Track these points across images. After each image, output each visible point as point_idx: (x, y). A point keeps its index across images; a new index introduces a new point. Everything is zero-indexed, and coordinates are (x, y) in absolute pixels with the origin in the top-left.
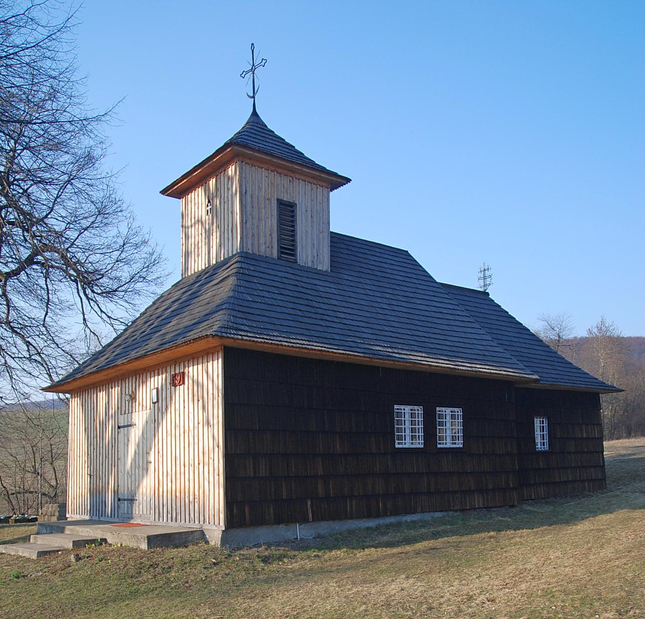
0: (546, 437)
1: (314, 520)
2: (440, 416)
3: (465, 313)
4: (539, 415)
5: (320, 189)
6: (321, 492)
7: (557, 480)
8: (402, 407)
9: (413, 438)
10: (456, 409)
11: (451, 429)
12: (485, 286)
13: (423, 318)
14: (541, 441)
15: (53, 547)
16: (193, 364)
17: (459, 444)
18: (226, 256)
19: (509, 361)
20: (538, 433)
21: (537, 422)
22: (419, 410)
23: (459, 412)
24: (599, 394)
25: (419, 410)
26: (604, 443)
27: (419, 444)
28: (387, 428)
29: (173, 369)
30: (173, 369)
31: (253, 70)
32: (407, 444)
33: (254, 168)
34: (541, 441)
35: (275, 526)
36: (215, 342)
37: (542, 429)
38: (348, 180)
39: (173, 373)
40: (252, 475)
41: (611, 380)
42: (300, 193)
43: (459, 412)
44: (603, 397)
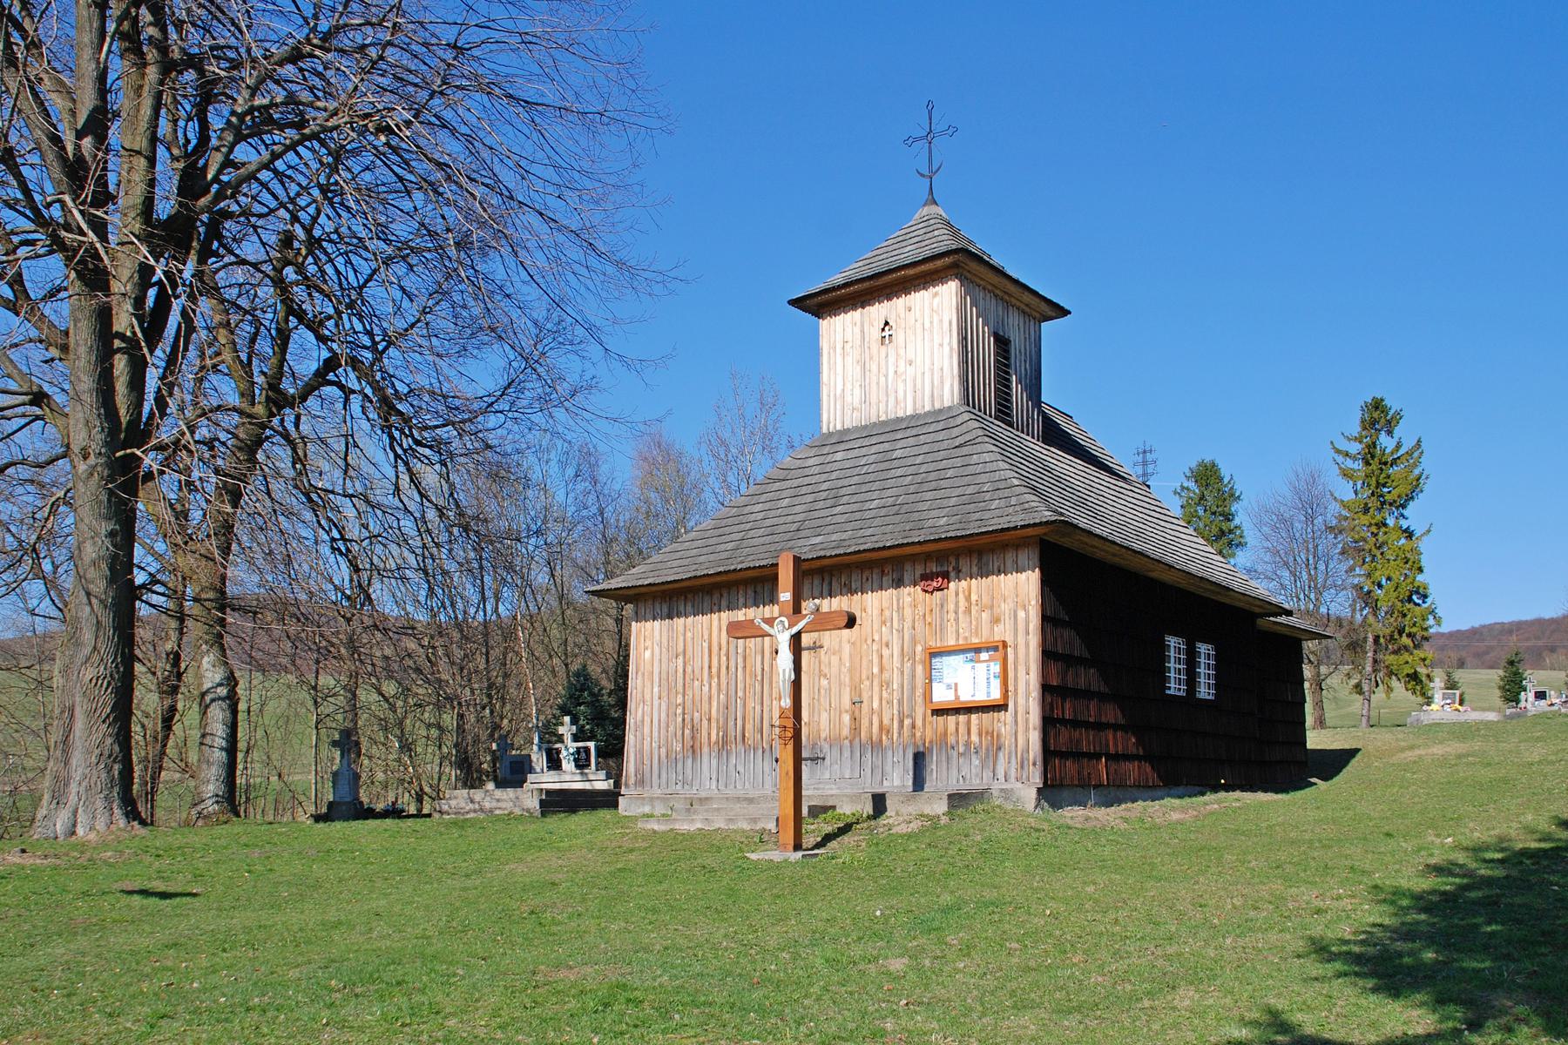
12: (1144, 475)
24: (1300, 641)
31: (929, 136)
38: (1064, 312)
44: (1309, 646)
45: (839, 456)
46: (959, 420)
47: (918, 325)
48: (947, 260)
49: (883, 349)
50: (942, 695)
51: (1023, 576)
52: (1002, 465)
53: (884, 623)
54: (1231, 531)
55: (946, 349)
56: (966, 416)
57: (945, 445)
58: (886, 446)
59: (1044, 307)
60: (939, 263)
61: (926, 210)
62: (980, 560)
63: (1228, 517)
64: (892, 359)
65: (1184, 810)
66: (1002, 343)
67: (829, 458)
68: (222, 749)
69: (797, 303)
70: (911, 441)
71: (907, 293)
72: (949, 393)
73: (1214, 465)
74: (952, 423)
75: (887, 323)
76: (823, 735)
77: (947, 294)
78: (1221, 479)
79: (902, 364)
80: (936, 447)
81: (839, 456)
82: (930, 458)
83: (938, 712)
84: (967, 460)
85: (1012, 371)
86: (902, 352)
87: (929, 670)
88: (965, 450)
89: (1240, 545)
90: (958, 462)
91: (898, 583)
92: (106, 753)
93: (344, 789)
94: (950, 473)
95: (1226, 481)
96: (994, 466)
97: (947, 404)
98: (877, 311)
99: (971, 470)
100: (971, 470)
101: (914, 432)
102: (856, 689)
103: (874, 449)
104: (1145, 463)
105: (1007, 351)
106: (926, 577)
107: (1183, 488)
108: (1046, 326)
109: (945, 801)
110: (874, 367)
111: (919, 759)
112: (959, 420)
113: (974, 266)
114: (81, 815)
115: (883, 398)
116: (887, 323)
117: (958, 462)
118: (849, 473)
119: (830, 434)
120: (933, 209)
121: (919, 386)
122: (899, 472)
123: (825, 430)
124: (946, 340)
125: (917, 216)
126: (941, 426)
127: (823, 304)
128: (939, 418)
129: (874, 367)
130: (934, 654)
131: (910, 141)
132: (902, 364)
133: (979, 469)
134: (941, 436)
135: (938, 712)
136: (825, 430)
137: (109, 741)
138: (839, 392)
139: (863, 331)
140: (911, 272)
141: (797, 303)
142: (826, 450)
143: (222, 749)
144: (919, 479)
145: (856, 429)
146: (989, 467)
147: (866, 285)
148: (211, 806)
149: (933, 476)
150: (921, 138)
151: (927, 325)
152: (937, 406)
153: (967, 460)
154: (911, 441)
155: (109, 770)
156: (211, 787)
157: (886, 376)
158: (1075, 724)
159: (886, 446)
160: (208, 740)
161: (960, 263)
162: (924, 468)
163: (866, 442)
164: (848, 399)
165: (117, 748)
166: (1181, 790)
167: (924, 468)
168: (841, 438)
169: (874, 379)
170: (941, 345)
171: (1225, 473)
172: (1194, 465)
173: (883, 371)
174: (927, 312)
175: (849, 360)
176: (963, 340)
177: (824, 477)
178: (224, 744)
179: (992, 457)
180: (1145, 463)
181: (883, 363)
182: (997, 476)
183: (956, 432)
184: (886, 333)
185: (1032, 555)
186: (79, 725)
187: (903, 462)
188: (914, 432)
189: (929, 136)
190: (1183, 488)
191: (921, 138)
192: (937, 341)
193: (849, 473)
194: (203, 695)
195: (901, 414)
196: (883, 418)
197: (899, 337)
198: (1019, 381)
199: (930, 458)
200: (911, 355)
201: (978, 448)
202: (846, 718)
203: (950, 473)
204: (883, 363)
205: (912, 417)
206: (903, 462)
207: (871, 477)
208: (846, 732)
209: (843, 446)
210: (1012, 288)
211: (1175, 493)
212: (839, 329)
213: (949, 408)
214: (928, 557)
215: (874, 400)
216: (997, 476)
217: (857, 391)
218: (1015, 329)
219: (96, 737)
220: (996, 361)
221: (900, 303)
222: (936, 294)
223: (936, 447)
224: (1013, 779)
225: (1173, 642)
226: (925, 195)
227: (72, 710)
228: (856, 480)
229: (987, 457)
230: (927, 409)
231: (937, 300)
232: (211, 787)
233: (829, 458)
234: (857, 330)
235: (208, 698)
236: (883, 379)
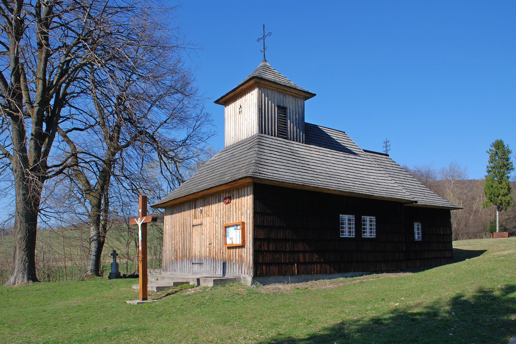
0: (420, 233)
1: (298, 273)
2: (364, 221)
3: (377, 166)
4: (417, 221)
5: (299, 100)
6: (302, 260)
7: (426, 257)
8: (344, 216)
9: (350, 232)
10: (372, 217)
11: (369, 231)
12: (386, 151)
13: (354, 168)
14: (417, 236)
15: (178, 279)
16: (195, 206)
17: (374, 235)
18: (252, 135)
19: (401, 191)
20: (416, 231)
21: (416, 225)
22: (352, 217)
23: (373, 218)
24: (449, 210)
25: (352, 217)
26: (453, 242)
27: (353, 235)
28: (337, 225)
29: (224, 195)
30: (224, 195)
31: (264, 37)
32: (346, 235)
33: (265, 89)
34: (417, 236)
35: (278, 276)
36: (250, 180)
37: (418, 229)
38: (315, 95)
39: (224, 197)
40: (266, 249)
41: (456, 204)
42: (290, 103)
43: (373, 218)
44: (452, 212)
50: (229, 242)
51: (249, 197)
53: (216, 215)
54: (508, 164)
62: (238, 192)
63: (507, 160)
65: (373, 278)
68: (94, 255)
69: (217, 102)
73: (501, 141)
76: (203, 255)
78: (504, 146)
83: (229, 248)
87: (226, 230)
89: (512, 169)
91: (219, 201)
92: (23, 260)
93: (114, 269)
95: (506, 146)
102: (210, 239)
104: (386, 146)
106: (225, 199)
107: (490, 150)
109: (212, 282)
111: (224, 264)
113: (263, 82)
114: (17, 278)
130: (226, 227)
131: (259, 40)
135: (229, 248)
137: (24, 256)
141: (217, 102)
143: (94, 255)
148: (89, 273)
150: (262, 38)
155: (24, 265)
156: (90, 267)
158: (276, 252)
160: (90, 253)
161: (257, 82)
165: (27, 258)
166: (351, 274)
171: (505, 144)
172: (494, 142)
176: (260, 110)
178: (95, 254)
180: (386, 146)
185: (250, 190)
186: (17, 252)
189: (264, 37)
190: (490, 150)
192: (253, 111)
194: (90, 239)
200: (246, 118)
202: (208, 249)
208: (208, 254)
211: (487, 152)
214: (226, 191)
218: (290, 103)
219: (21, 255)
221: (244, 98)
224: (246, 274)
225: (345, 218)
226: (263, 58)
227: (16, 247)
232: (90, 267)
235: (91, 240)
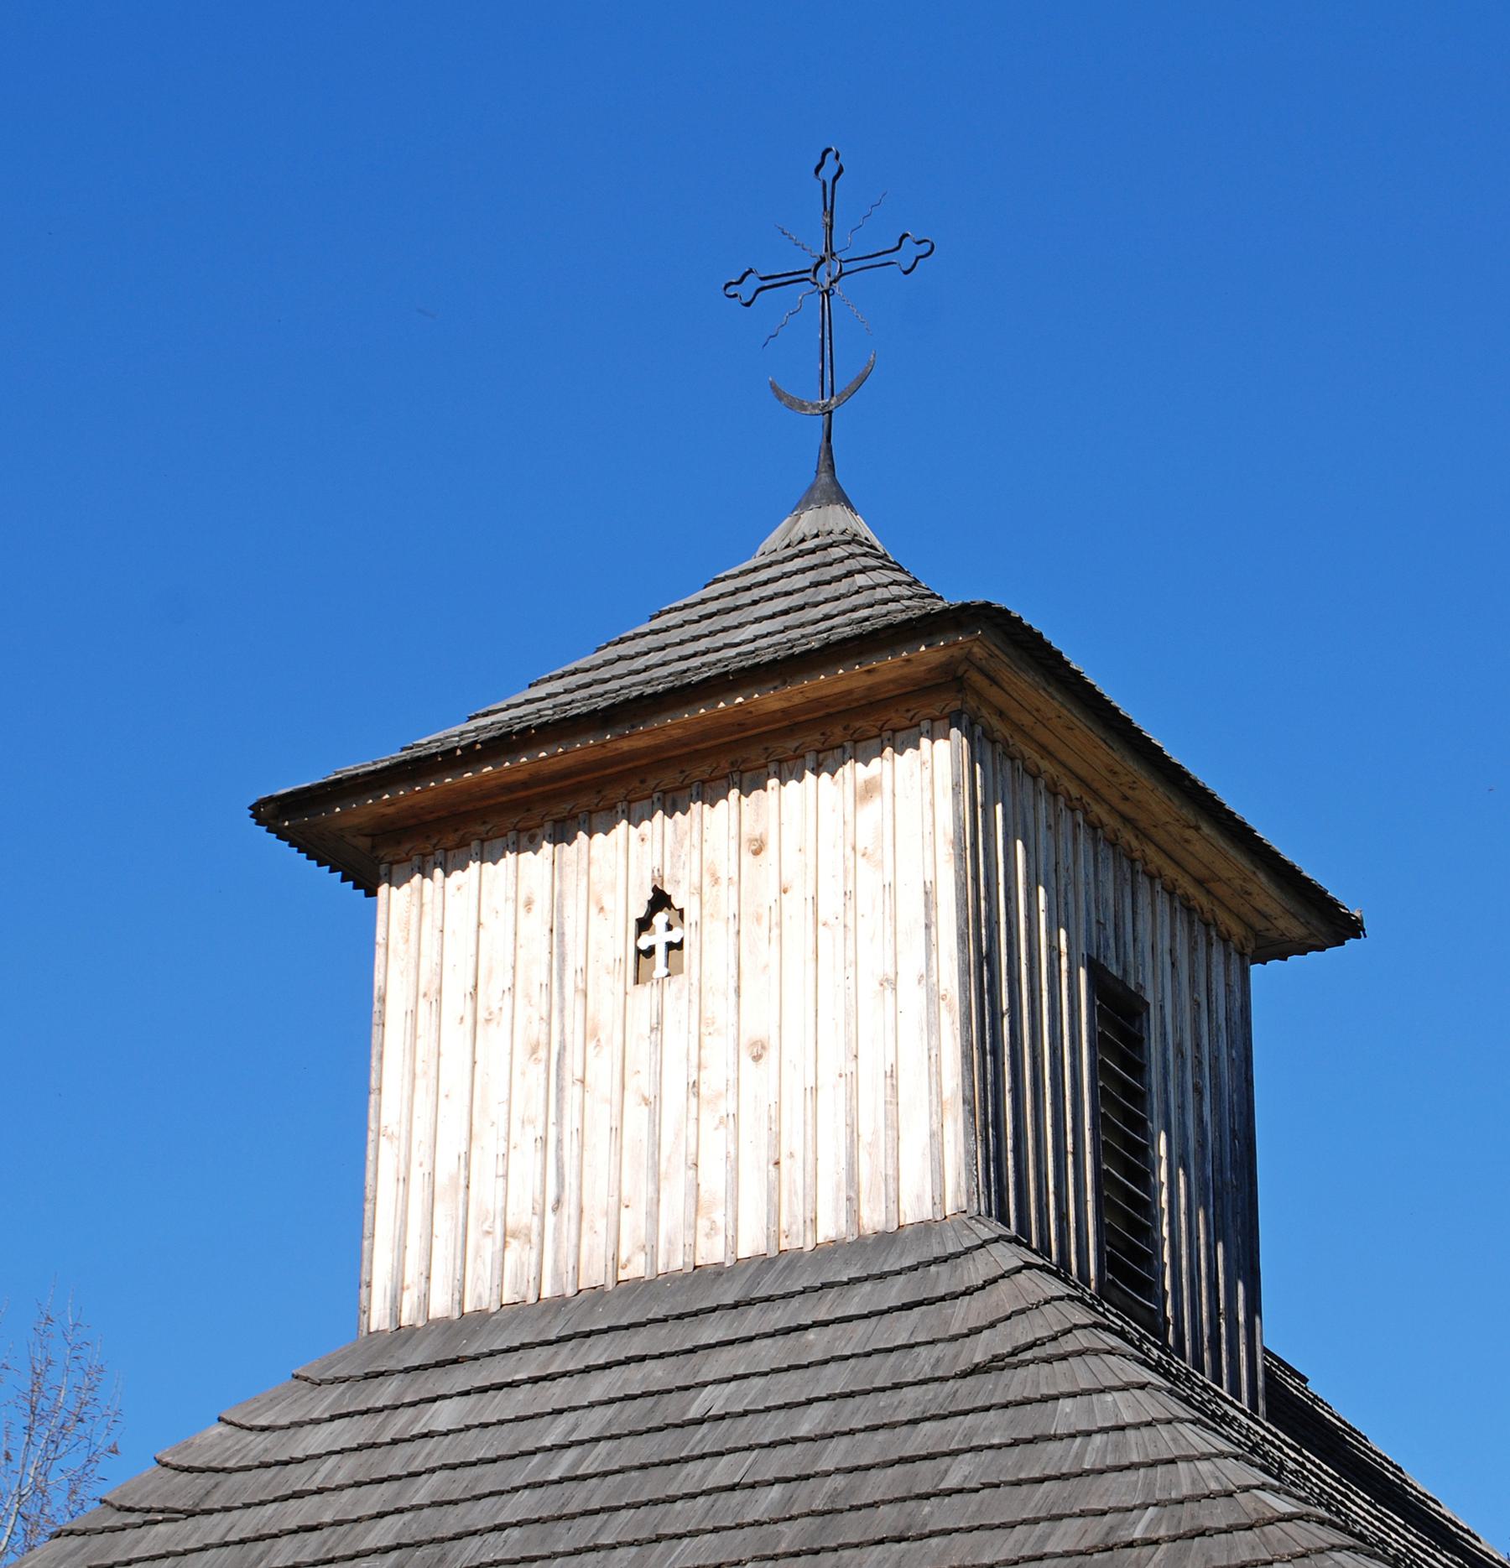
38: (1339, 926)
45: (444, 1415)
46: (976, 1270)
47: (795, 905)
48: (925, 654)
49: (644, 995)
52: (1197, 1439)
55: (913, 997)
56: (1007, 1256)
57: (923, 1362)
58: (657, 1374)
59: (1266, 895)
60: (889, 666)
61: (808, 522)
64: (677, 1038)
66: (1119, 1014)
67: (399, 1424)
70: (768, 1353)
71: (751, 782)
72: (921, 1165)
74: (943, 1280)
75: (660, 900)
77: (923, 783)
79: (719, 1052)
80: (883, 1371)
81: (444, 1415)
82: (858, 1413)
84: (1030, 1421)
85: (1155, 1125)
86: (719, 1007)
88: (1017, 1383)
90: (995, 1428)
94: (958, 1473)
96: (1163, 1442)
97: (915, 1209)
98: (617, 860)
99: (1051, 1458)
100: (1051, 1458)
101: (779, 1316)
103: (600, 1386)
105: (1137, 1042)
108: (1269, 980)
110: (602, 1070)
112: (976, 1270)
113: (1023, 687)
115: (637, 1187)
116: (660, 900)
117: (995, 1428)
118: (490, 1478)
119: (402, 1335)
120: (837, 518)
121: (793, 1141)
122: (722, 1471)
123: (378, 1318)
124: (912, 960)
125: (774, 540)
126: (895, 1292)
127: (382, 825)
128: (879, 1267)
129: (602, 1070)
132: (719, 1052)
133: (1095, 1452)
134: (900, 1329)
136: (378, 1318)
138: (447, 1166)
139: (555, 931)
140: (769, 699)
141: (287, 815)
142: (386, 1392)
144: (818, 1495)
145: (515, 1312)
146: (1136, 1447)
147: (585, 746)
149: (877, 1485)
150: (796, 277)
151: (831, 905)
152: (874, 1219)
153: (1030, 1421)
154: (768, 1353)
157: (653, 1102)
159: (657, 1374)
161: (962, 671)
162: (834, 1454)
163: (563, 1358)
164: (486, 1192)
167: (834, 1454)
168: (454, 1348)
169: (600, 1119)
170: (890, 983)
173: (639, 1083)
174: (832, 859)
175: (494, 1041)
176: (982, 963)
177: (375, 1499)
179: (1125, 1408)
181: (639, 1052)
182: (1184, 1479)
183: (962, 1315)
184: (658, 937)
187: (740, 1431)
188: (779, 1316)
191: (796, 277)
192: (874, 963)
193: (490, 1478)
195: (712, 1252)
196: (637, 1268)
197: (709, 943)
198: (1179, 1160)
199: (858, 1413)
200: (758, 1022)
201: (1080, 1373)
203: (958, 1473)
204: (639, 1052)
205: (763, 1263)
206: (740, 1431)
207: (597, 1494)
209: (462, 1378)
210: (1155, 800)
212: (463, 942)
213: (925, 1228)
215: (598, 1196)
216: (1184, 1479)
217: (526, 1164)
220: (1098, 1068)
221: (718, 821)
222: (868, 791)
223: (883, 1371)
228: (523, 1505)
229: (1125, 1408)
230: (830, 1227)
231: (873, 811)
233: (399, 1424)
234: (535, 926)
236: (636, 1116)
